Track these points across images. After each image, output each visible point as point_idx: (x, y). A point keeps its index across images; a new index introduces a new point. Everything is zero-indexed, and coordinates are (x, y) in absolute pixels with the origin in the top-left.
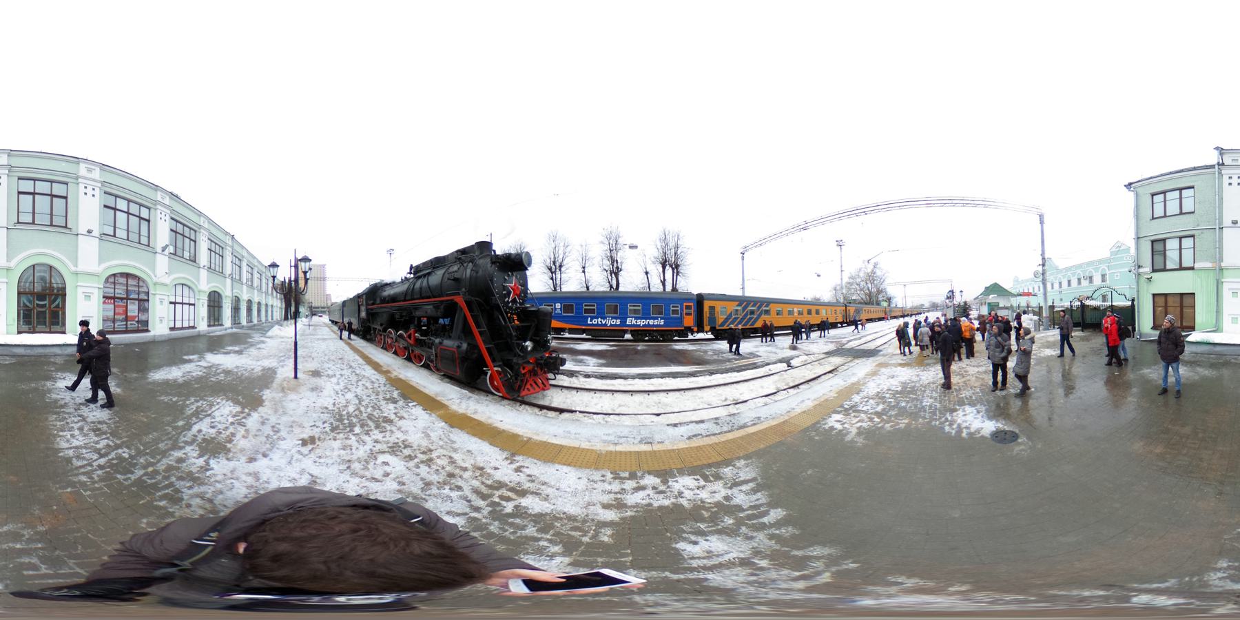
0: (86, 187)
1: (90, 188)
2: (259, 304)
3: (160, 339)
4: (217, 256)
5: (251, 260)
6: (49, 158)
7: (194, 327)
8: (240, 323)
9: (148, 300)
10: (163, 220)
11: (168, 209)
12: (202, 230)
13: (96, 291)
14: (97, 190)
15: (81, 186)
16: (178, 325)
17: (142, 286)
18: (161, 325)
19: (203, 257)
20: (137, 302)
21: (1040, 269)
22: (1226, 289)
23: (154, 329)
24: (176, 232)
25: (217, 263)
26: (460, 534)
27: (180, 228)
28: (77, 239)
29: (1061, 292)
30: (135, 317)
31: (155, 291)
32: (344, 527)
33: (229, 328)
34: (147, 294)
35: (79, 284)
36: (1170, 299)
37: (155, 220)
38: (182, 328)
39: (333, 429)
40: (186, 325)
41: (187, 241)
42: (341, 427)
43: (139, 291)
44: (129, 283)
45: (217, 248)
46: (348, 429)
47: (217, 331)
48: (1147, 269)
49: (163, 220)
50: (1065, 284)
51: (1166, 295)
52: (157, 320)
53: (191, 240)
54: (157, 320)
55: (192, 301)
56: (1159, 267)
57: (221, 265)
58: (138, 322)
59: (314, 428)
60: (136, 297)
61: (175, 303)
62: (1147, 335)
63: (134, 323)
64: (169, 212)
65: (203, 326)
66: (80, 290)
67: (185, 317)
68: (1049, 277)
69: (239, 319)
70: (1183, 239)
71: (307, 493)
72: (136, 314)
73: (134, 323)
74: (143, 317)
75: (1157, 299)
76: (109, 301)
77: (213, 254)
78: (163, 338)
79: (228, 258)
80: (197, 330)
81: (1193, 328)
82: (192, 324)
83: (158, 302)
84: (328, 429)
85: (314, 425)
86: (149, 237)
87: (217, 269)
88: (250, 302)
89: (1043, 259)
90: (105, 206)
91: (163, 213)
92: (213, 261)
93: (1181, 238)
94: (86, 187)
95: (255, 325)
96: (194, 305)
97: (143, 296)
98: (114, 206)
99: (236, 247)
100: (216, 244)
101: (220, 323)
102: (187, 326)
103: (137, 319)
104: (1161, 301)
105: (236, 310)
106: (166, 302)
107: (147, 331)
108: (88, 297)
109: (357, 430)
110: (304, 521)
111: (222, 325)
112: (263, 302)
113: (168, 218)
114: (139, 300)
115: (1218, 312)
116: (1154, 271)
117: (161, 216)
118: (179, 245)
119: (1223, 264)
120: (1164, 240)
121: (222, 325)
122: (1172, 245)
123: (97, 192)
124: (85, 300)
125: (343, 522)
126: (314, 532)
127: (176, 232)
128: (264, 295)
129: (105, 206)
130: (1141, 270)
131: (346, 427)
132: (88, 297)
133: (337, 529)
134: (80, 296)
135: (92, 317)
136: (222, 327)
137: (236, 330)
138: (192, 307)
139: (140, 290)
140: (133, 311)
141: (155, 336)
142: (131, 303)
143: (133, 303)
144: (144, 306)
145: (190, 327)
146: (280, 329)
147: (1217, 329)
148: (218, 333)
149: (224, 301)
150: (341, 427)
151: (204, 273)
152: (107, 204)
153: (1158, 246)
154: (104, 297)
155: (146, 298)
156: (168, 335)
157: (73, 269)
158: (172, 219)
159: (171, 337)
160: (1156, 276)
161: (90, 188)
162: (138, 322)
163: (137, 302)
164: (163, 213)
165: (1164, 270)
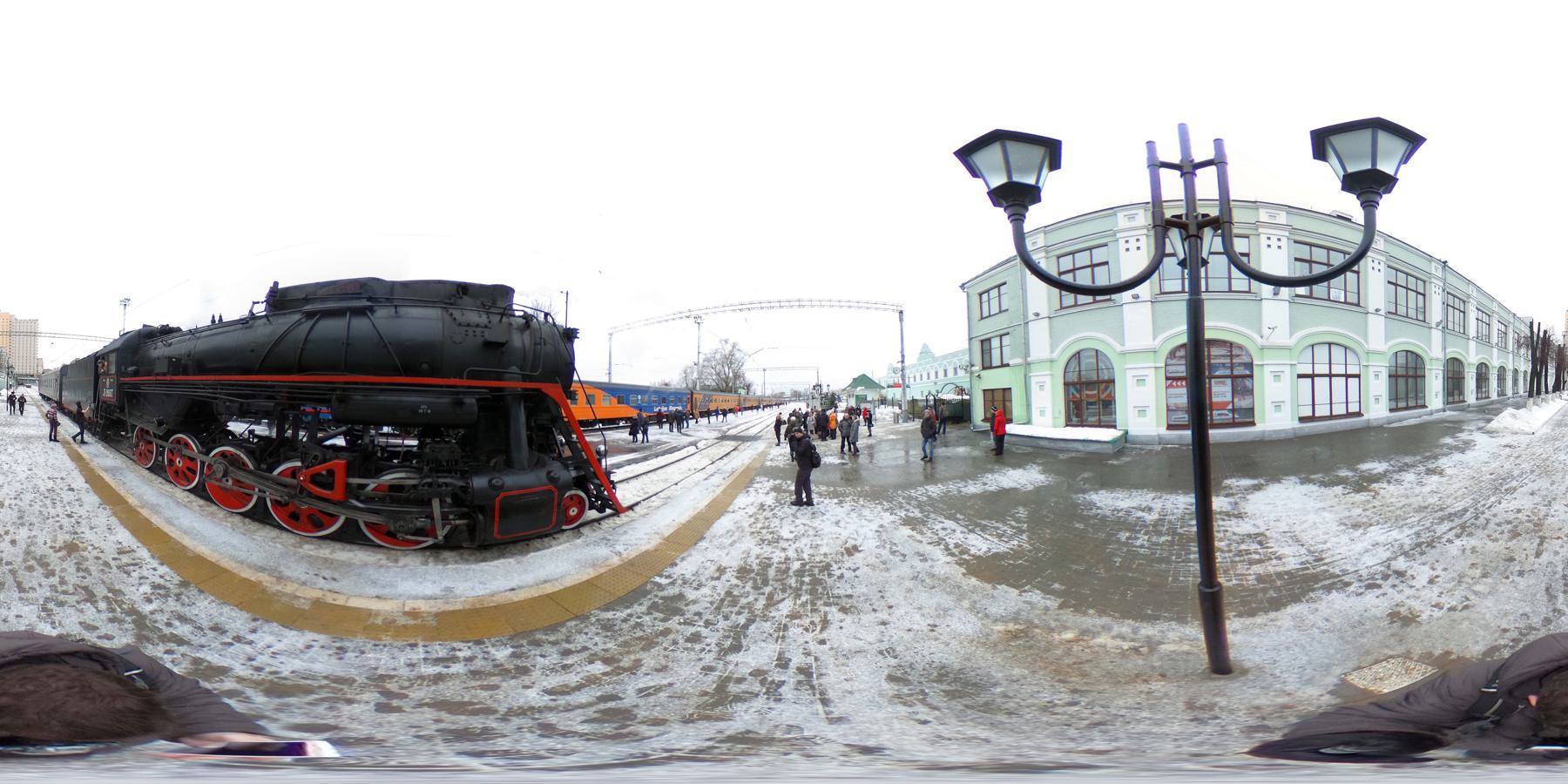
0: (1269, 238)
1: (1274, 239)
2: (1502, 370)
3: (1274, 437)
4: (1457, 312)
5: (1504, 315)
6: (1083, 222)
7: (1359, 414)
8: (1464, 401)
9: (1251, 376)
10: (1376, 270)
11: (1383, 255)
12: (1433, 280)
13: (1152, 373)
14: (1284, 240)
15: (1263, 238)
16: (1322, 411)
17: (1238, 356)
18: (1378, 406)
19: (1436, 313)
20: (1229, 381)
21: (900, 365)
22: (1034, 381)
23: (1263, 421)
24: (1396, 285)
25: (1457, 321)
26: (199, 690)
27: (1402, 279)
28: (1122, 311)
29: (935, 383)
30: (1228, 403)
31: (1368, 361)
32: (61, 684)
33: (1438, 411)
34: (1250, 366)
35: (1127, 366)
36: (996, 394)
37: (1366, 271)
38: (1331, 417)
39: (827, 567)
40: (1339, 409)
41: (1412, 295)
42: (816, 571)
43: (1232, 363)
44: (1212, 353)
45: (1456, 302)
46: (807, 567)
47: (1411, 418)
48: (977, 368)
49: (1376, 270)
50: (925, 377)
51: (993, 390)
52: (1372, 400)
53: (1418, 293)
54: (1269, 407)
55: (1352, 370)
56: (987, 366)
57: (1462, 324)
58: (1233, 411)
59: (853, 567)
60: (1228, 372)
61: (1312, 376)
62: (979, 426)
63: (1225, 412)
64: (1384, 259)
65: (1378, 410)
66: (1130, 374)
67: (1332, 398)
68: (907, 372)
69: (1461, 393)
70: (1004, 338)
71: (29, 638)
72: (1229, 398)
73: (1225, 412)
74: (1242, 403)
75: (987, 393)
76: (1179, 383)
77: (1450, 309)
78: (1283, 436)
79: (1472, 315)
80: (1366, 417)
81: (1010, 421)
82: (1353, 408)
83: (1372, 376)
84: (835, 567)
85: (854, 571)
86: (1359, 294)
87: (1457, 329)
88: (1502, 370)
89: (903, 356)
90: (1296, 259)
91: (1376, 261)
92: (1450, 318)
93: (1001, 336)
94: (1269, 238)
95: (1492, 403)
96: (1358, 376)
97: (1239, 371)
98: (1308, 258)
99: (1451, 279)
100: (1454, 296)
101: (1420, 402)
102: (1344, 412)
103: (1230, 407)
104: (989, 395)
105: (1482, 378)
106: (1288, 376)
107: (1253, 424)
108: (1277, 377)
109: (796, 565)
110: (25, 678)
111: (1424, 406)
112: (1510, 367)
113: (1382, 267)
114: (1233, 377)
115: (1028, 406)
116: (984, 368)
117: (1373, 265)
118: (1401, 301)
119: (1029, 359)
120: (989, 339)
121: (1424, 406)
122: (995, 343)
123: (1284, 242)
124: (1138, 385)
125: (62, 679)
126: (32, 688)
127: (1396, 285)
128: (1511, 355)
129: (1296, 259)
130: (973, 368)
131: (809, 570)
132: (1277, 377)
133: (54, 686)
134: (1131, 382)
135: (1283, 402)
136: (1424, 410)
137: (1452, 413)
138: (1353, 382)
139: (1234, 361)
140: (1223, 394)
141: (1264, 432)
142: (1217, 383)
143: (1223, 383)
144: (1245, 387)
145: (1348, 415)
146: (1514, 416)
147: (1029, 422)
148: (1412, 422)
149: (1466, 370)
150: (816, 571)
151: (1472, 344)
152: (1298, 256)
153: (985, 343)
154: (1167, 378)
155: (1248, 372)
156: (1294, 429)
157: (1119, 348)
158: (1389, 267)
159: (1300, 433)
160: (984, 373)
161: (1274, 239)
162: (1233, 411)
163: (1229, 381)
164: (1376, 261)
165: (991, 367)
